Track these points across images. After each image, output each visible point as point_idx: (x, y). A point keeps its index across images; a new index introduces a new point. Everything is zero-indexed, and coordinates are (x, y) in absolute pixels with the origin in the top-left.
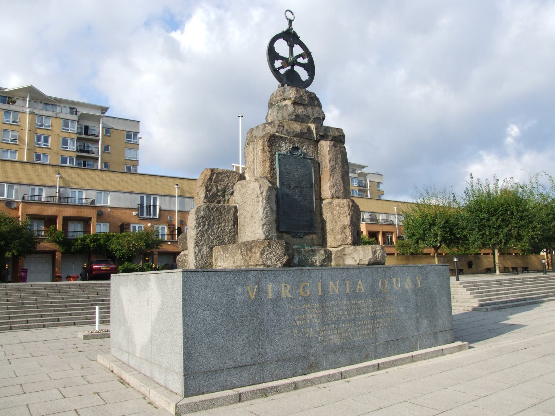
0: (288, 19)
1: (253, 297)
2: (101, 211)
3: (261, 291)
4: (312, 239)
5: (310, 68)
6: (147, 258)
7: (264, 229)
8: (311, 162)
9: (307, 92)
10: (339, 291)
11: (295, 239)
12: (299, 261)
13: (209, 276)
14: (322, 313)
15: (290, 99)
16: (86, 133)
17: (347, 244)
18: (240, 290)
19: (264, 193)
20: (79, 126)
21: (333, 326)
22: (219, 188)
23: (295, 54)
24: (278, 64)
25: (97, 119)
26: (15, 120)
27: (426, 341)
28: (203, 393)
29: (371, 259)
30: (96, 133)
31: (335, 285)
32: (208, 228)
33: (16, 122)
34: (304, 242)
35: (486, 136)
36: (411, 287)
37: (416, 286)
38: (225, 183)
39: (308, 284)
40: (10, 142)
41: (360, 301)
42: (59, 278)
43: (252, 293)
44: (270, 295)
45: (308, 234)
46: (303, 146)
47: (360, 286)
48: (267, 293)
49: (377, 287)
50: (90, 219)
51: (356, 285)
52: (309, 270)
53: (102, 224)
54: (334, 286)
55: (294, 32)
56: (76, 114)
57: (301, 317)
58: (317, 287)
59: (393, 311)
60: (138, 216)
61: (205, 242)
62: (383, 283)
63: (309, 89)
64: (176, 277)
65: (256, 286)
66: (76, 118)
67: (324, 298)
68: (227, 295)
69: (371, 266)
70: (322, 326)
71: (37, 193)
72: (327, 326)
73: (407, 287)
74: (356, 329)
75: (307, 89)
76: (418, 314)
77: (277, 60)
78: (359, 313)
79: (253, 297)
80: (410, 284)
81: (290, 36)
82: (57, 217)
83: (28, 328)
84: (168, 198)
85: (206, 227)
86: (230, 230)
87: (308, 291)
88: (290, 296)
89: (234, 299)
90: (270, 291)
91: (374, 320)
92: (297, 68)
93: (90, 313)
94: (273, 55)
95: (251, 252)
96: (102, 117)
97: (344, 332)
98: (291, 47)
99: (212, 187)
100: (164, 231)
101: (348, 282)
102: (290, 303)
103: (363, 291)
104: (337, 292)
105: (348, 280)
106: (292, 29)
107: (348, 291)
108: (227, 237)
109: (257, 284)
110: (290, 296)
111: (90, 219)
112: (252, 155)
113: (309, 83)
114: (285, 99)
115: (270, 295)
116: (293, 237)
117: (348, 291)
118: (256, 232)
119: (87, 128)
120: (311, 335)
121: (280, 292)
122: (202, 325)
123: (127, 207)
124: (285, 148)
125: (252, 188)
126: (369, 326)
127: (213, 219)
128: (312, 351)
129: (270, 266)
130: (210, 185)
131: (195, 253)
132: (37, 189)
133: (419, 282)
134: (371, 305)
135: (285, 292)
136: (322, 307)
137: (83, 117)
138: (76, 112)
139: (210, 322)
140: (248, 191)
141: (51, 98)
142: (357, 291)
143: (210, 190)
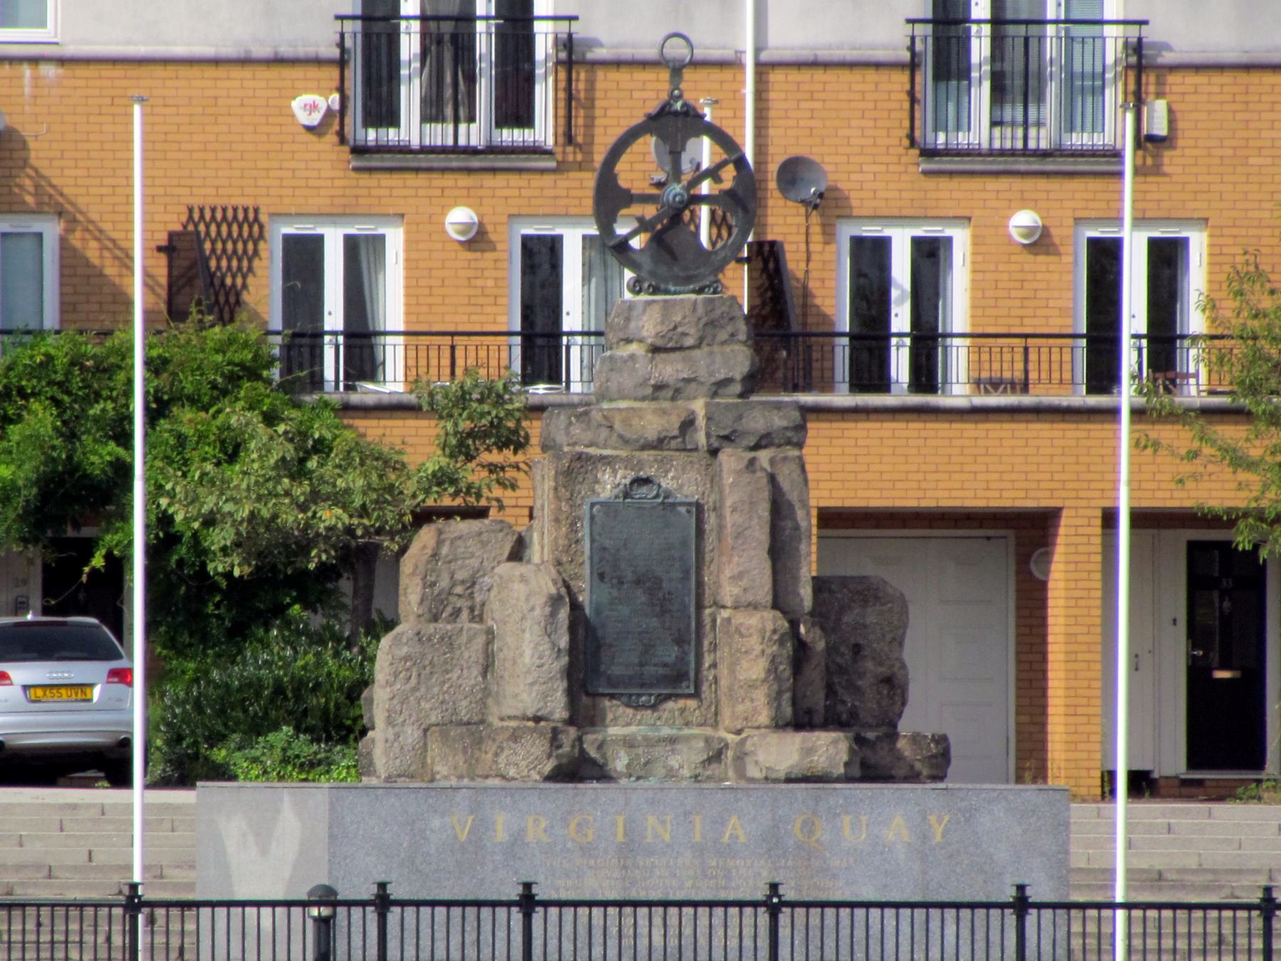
4: (682, 711)
7: (534, 694)
8: (689, 512)
10: (672, 837)
12: (628, 766)
13: (377, 797)
14: (624, 879)
15: (641, 341)
17: (758, 728)
19: (537, 612)
22: (460, 576)
29: (792, 767)
31: (663, 822)
32: (419, 683)
35: (557, 790)
36: (906, 839)
37: (925, 838)
38: (474, 563)
39: (591, 818)
41: (731, 864)
43: (463, 830)
45: (668, 697)
46: (667, 472)
48: (495, 831)
51: (723, 824)
52: (595, 789)
57: (570, 883)
58: (614, 824)
61: (410, 716)
65: (471, 818)
69: (791, 786)
73: (891, 836)
79: (463, 837)
85: (414, 681)
86: (473, 687)
87: (590, 832)
88: (545, 839)
89: (424, 838)
90: (499, 827)
99: (438, 576)
103: (742, 839)
105: (698, 813)
107: (698, 838)
108: (464, 703)
110: (545, 839)
114: (628, 341)
115: (501, 835)
117: (698, 838)
123: (228, 51)
124: (609, 484)
127: (431, 662)
129: (513, 779)
130: (433, 571)
131: (387, 741)
133: (939, 830)
136: (625, 867)
142: (726, 839)
143: (433, 584)
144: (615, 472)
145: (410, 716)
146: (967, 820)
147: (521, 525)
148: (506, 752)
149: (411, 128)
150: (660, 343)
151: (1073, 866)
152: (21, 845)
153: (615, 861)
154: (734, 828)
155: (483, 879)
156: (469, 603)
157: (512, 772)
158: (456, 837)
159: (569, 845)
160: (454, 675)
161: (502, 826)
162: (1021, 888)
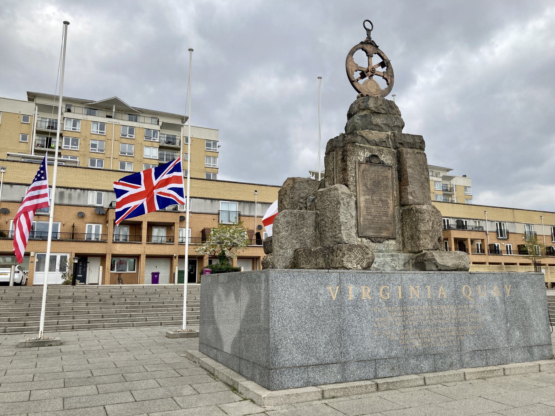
1: (334, 298)
3: (342, 292)
22: (302, 195)
28: (288, 388)
31: (416, 289)
37: (504, 294)
39: (388, 287)
43: (334, 294)
44: (351, 297)
46: (382, 155)
50: (173, 224)
58: (397, 290)
68: (311, 294)
74: (438, 335)
75: (386, 98)
76: (508, 324)
79: (334, 298)
81: (368, 45)
87: (388, 294)
90: (350, 292)
95: (333, 255)
97: (426, 338)
98: (369, 56)
101: (429, 287)
102: (371, 305)
103: (445, 297)
108: (309, 241)
111: (173, 224)
115: (351, 297)
122: (288, 322)
125: (333, 196)
129: (350, 269)
135: (366, 294)
136: (403, 311)
141: (135, 108)
142: (439, 297)
146: (517, 287)
148: (347, 256)
150: (376, 110)
151: (34, 284)
152: (321, 78)
155: (344, 319)
157: (349, 265)
158: (331, 297)
159: (380, 300)
160: (305, 230)
161: (352, 290)
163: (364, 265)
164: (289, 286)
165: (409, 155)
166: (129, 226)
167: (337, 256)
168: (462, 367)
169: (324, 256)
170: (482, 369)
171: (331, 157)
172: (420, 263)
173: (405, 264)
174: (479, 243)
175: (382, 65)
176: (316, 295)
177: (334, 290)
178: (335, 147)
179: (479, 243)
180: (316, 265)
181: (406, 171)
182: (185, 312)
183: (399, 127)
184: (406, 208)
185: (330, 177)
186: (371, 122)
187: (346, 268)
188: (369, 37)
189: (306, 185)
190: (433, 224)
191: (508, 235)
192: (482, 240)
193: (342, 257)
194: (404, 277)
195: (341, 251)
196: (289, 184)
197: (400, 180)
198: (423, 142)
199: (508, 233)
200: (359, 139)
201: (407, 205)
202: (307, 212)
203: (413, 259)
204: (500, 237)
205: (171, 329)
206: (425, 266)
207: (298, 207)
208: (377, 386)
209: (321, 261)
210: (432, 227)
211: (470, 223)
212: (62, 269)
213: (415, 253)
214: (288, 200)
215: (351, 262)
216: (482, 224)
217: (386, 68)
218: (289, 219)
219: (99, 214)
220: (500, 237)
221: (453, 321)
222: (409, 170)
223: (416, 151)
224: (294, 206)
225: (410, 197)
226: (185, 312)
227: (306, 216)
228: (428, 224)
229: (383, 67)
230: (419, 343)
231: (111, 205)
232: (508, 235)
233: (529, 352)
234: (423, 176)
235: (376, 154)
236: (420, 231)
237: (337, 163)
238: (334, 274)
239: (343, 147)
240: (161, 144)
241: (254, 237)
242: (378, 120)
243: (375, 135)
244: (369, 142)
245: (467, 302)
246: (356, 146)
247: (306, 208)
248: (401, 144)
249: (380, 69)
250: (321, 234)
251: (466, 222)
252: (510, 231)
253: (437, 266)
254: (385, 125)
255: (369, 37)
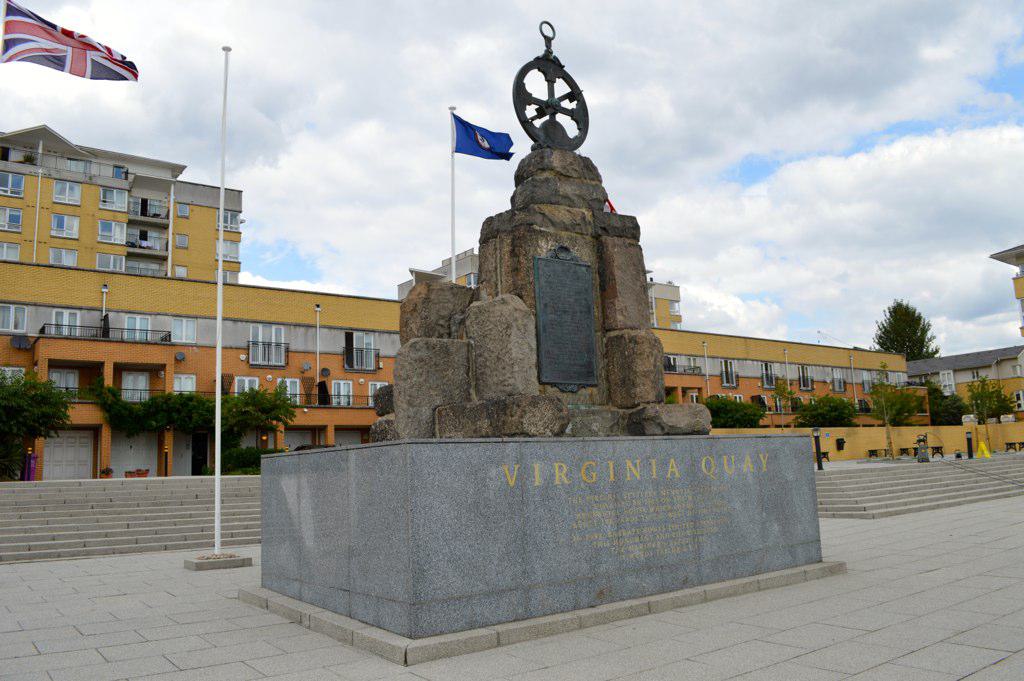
0: (543, 35)
1: (512, 483)
2: (182, 354)
3: (525, 474)
4: (591, 395)
5: (581, 116)
6: (264, 438)
9: (575, 155)
11: (565, 395)
16: (144, 212)
18: (493, 472)
20: (131, 200)
21: (634, 530)
23: (558, 94)
24: (531, 111)
25: (162, 186)
26: (16, 189)
27: (778, 559)
28: (442, 633)
30: (163, 213)
31: (635, 465)
33: (18, 193)
34: (579, 399)
40: (6, 229)
42: (107, 473)
44: (538, 481)
47: (672, 467)
49: (700, 470)
50: (163, 367)
52: (594, 441)
53: (183, 377)
54: (633, 469)
55: (555, 57)
56: (126, 178)
59: (725, 509)
60: (248, 362)
62: (708, 463)
63: (582, 151)
64: (397, 453)
65: (516, 467)
66: (125, 184)
67: (618, 486)
68: (476, 479)
70: (617, 531)
71: (66, 320)
72: (623, 530)
74: (667, 535)
75: (577, 152)
77: (530, 105)
78: (671, 511)
79: (512, 483)
80: (751, 466)
81: (549, 65)
82: (102, 364)
83: (88, 554)
84: (302, 329)
88: (566, 482)
90: (537, 473)
91: (695, 522)
92: (560, 118)
93: (206, 522)
94: (521, 97)
95: (506, 414)
96: (174, 183)
98: (551, 82)
100: (294, 387)
104: (638, 477)
106: (552, 53)
109: (518, 463)
110: (566, 482)
111: (163, 367)
112: (493, 261)
113: (580, 140)
114: (543, 170)
115: (538, 481)
116: (563, 391)
118: (506, 383)
119: (144, 202)
120: (600, 544)
121: (553, 475)
125: (499, 313)
126: (688, 532)
128: (602, 569)
132: (66, 313)
133: (764, 462)
134: (690, 498)
135: (560, 476)
137: (140, 181)
138: (127, 173)
139: (450, 522)
140: (492, 319)
141: (81, 148)
144: (548, 241)
145: (424, 399)
147: (166, 205)
148: (528, 415)
149: (802, 388)
153: (610, 496)
154: (672, 467)
156: (447, 331)
157: (533, 430)
160: (450, 373)
162: (548, 156)
163: (556, 428)
164: (440, 468)
165: (615, 247)
166: (77, 372)
167: (512, 416)
168: (701, 583)
169: (489, 416)
170: (786, 572)
171: (491, 247)
172: (636, 425)
173: (611, 427)
174: (694, 395)
175: (571, 97)
176: (484, 479)
177: (511, 471)
178: (498, 231)
179: (694, 395)
180: (475, 431)
181: (612, 274)
182: (217, 524)
183: (599, 201)
184: (613, 334)
185: (489, 281)
186: (557, 191)
187: (527, 435)
188: (549, 51)
189: (449, 296)
190: (655, 360)
191: (737, 381)
192: (700, 389)
193: (522, 417)
194: (618, 446)
195: (518, 406)
196: (420, 293)
197: (603, 289)
198: (637, 227)
199: (737, 376)
200: (539, 218)
201: (615, 330)
202: (453, 342)
203: (623, 419)
204: (725, 384)
205: (194, 555)
206: (643, 428)
207: (437, 334)
208: (406, 661)
209: (484, 424)
210: (655, 366)
211: (681, 362)
212: (909, 384)
213: (628, 408)
214: (418, 320)
215: (537, 420)
216: (699, 362)
217: (576, 102)
218: (423, 353)
219: (19, 349)
220: (725, 384)
221: (689, 514)
222: (618, 273)
223: (628, 241)
224: (429, 331)
225: (620, 317)
226: (217, 524)
227: (453, 349)
228: (649, 361)
229: (571, 101)
230: (640, 550)
231: (42, 331)
232: (737, 381)
233: (790, 552)
234: (639, 283)
235: (566, 245)
236: (635, 372)
237: (501, 259)
238: (511, 447)
239: (512, 231)
240: (132, 217)
241: (316, 391)
242: (567, 189)
243: (561, 213)
244: (553, 224)
245: (708, 483)
246: (535, 231)
247: (449, 335)
248: (604, 229)
249: (566, 104)
250: (477, 379)
251: (674, 359)
252: (740, 374)
253: (663, 429)
254: (579, 196)
255: (549, 51)
